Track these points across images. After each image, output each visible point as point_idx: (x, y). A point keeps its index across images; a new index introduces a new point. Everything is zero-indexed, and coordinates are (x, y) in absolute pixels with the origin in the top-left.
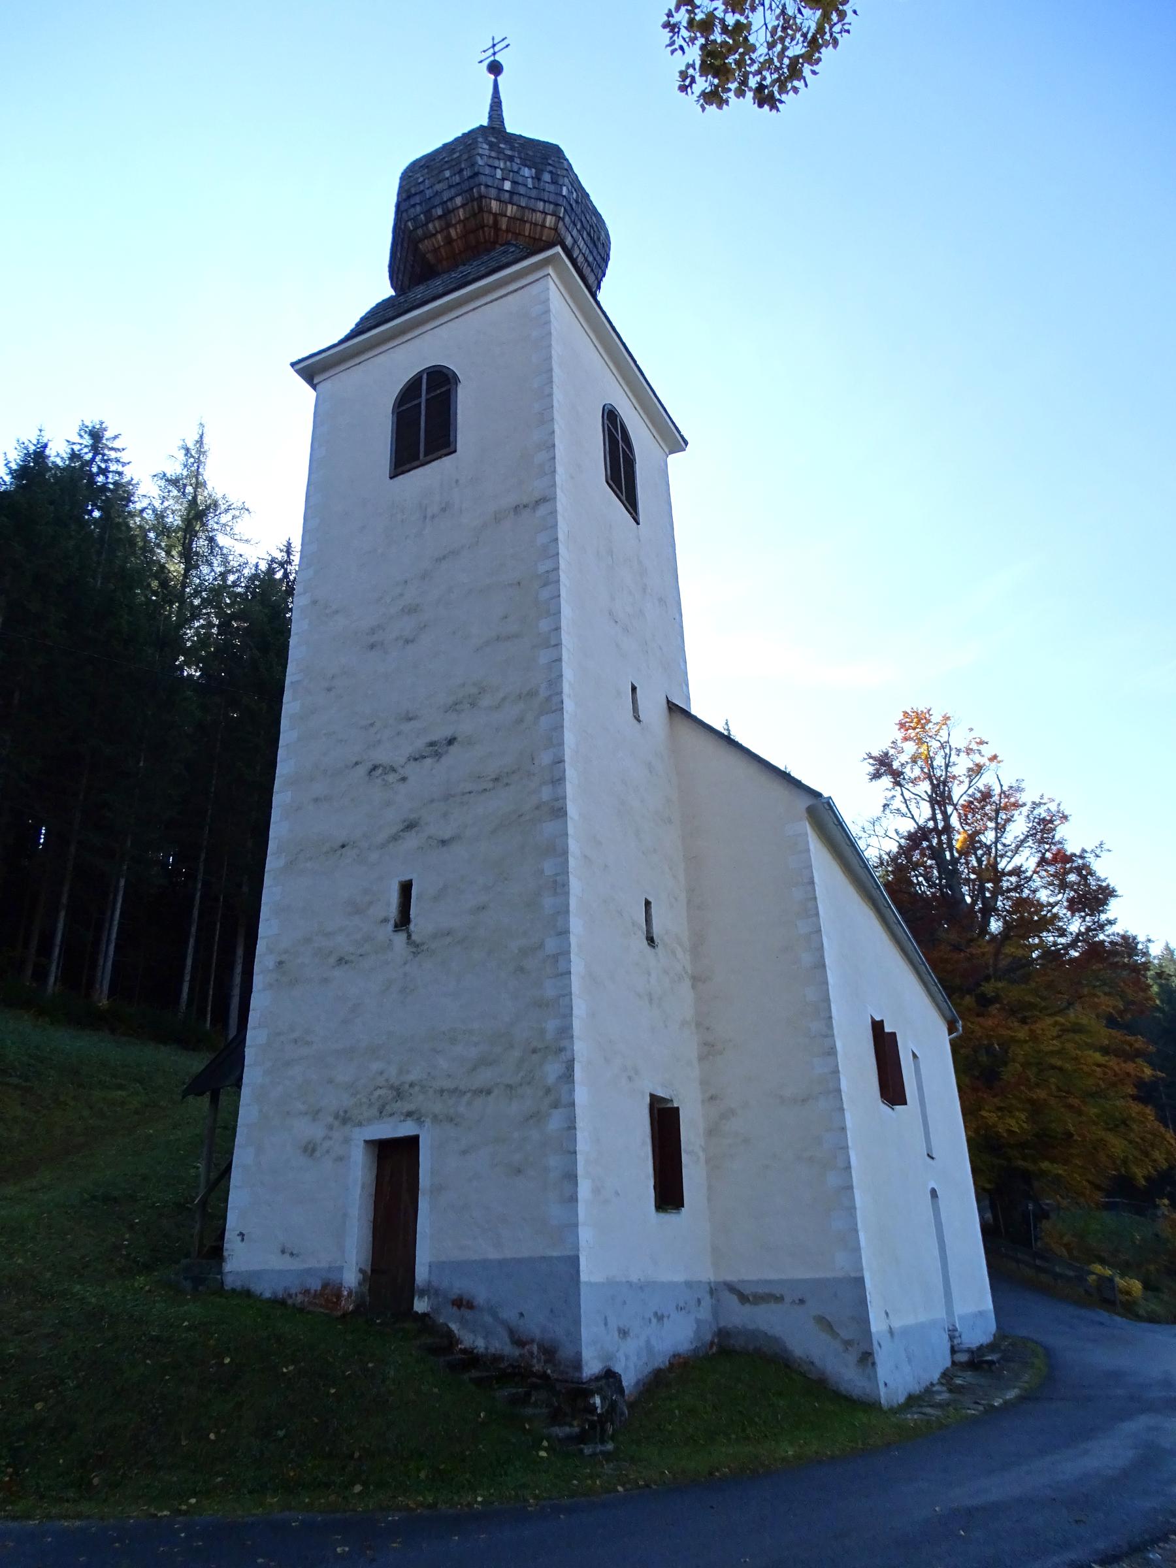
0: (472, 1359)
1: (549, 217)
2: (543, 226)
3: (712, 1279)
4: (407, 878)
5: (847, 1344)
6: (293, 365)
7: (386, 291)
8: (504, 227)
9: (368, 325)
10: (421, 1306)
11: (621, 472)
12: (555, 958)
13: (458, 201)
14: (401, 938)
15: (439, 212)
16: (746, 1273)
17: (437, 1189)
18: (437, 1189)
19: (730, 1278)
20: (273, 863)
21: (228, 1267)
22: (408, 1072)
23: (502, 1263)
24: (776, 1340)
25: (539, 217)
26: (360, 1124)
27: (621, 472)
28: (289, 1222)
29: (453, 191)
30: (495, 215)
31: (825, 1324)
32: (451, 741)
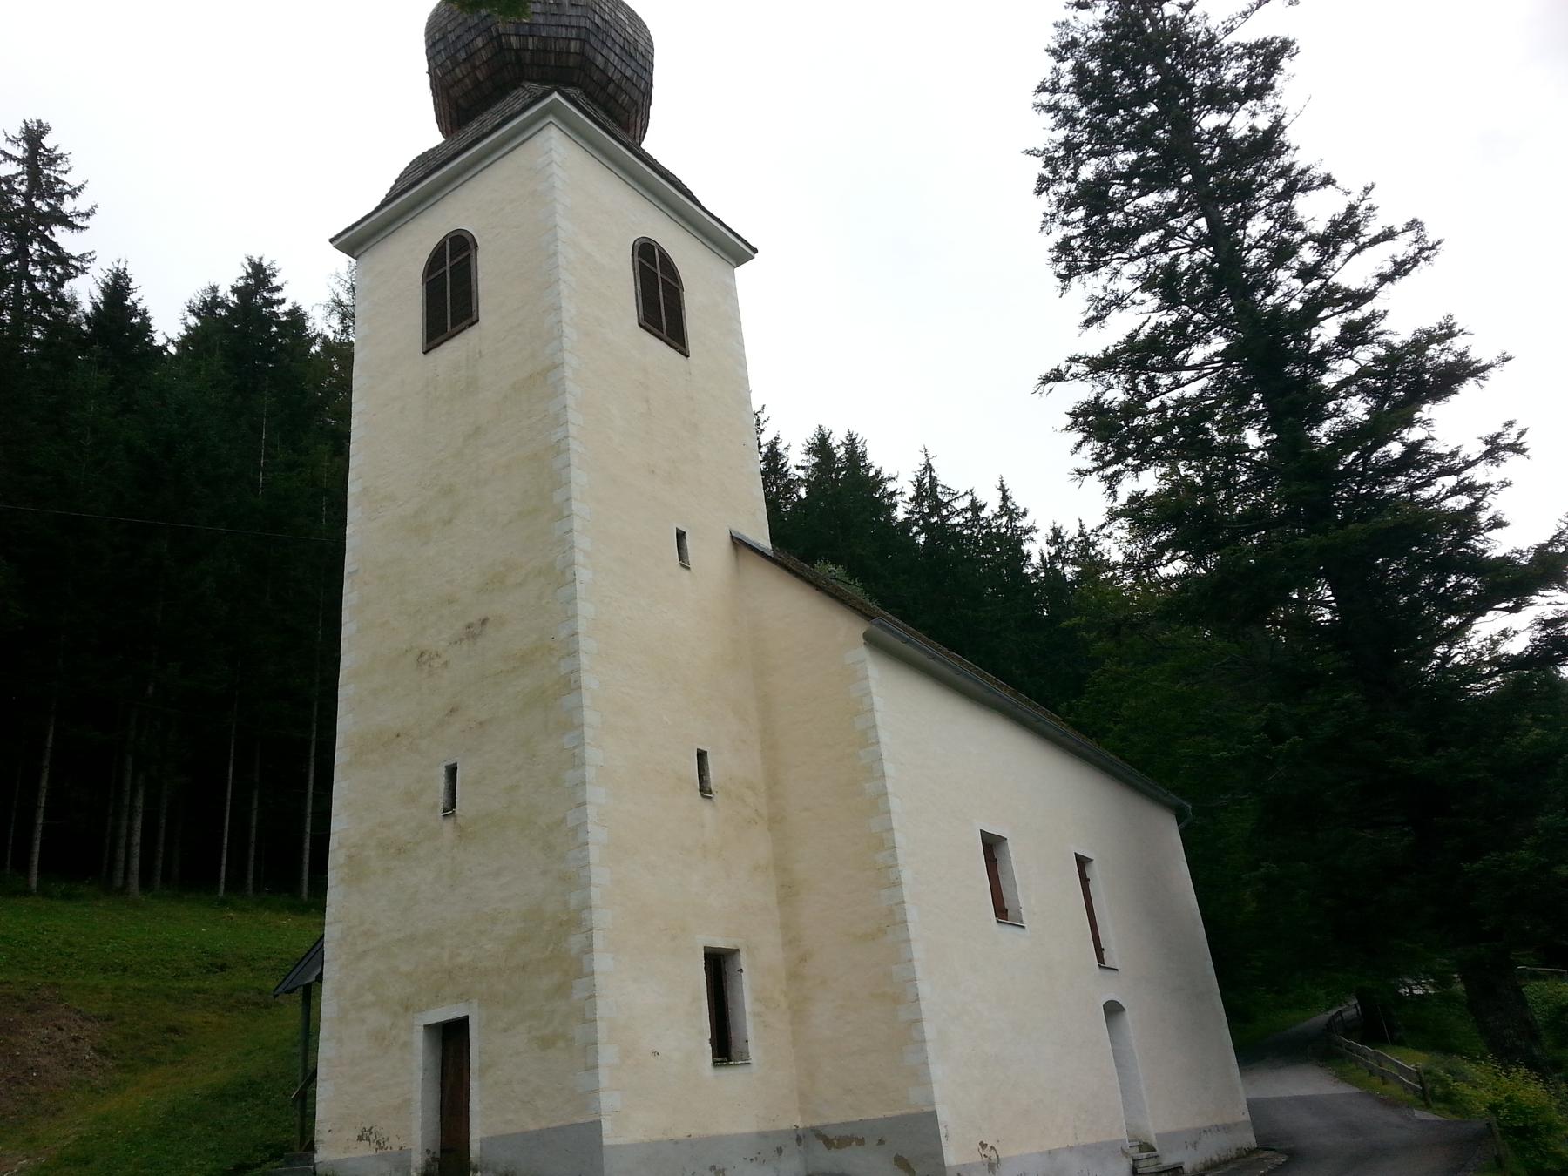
1: (573, 43)
2: (569, 53)
3: (801, 1126)
4: (451, 762)
6: (332, 241)
7: (432, 137)
8: (528, 60)
9: (410, 180)
11: (661, 304)
13: (479, 42)
14: (448, 825)
16: (834, 1115)
19: (816, 1123)
21: (318, 1158)
22: (459, 955)
23: (539, 1134)
25: (561, 45)
26: (420, 1011)
27: (661, 304)
30: (517, 50)
32: (484, 622)
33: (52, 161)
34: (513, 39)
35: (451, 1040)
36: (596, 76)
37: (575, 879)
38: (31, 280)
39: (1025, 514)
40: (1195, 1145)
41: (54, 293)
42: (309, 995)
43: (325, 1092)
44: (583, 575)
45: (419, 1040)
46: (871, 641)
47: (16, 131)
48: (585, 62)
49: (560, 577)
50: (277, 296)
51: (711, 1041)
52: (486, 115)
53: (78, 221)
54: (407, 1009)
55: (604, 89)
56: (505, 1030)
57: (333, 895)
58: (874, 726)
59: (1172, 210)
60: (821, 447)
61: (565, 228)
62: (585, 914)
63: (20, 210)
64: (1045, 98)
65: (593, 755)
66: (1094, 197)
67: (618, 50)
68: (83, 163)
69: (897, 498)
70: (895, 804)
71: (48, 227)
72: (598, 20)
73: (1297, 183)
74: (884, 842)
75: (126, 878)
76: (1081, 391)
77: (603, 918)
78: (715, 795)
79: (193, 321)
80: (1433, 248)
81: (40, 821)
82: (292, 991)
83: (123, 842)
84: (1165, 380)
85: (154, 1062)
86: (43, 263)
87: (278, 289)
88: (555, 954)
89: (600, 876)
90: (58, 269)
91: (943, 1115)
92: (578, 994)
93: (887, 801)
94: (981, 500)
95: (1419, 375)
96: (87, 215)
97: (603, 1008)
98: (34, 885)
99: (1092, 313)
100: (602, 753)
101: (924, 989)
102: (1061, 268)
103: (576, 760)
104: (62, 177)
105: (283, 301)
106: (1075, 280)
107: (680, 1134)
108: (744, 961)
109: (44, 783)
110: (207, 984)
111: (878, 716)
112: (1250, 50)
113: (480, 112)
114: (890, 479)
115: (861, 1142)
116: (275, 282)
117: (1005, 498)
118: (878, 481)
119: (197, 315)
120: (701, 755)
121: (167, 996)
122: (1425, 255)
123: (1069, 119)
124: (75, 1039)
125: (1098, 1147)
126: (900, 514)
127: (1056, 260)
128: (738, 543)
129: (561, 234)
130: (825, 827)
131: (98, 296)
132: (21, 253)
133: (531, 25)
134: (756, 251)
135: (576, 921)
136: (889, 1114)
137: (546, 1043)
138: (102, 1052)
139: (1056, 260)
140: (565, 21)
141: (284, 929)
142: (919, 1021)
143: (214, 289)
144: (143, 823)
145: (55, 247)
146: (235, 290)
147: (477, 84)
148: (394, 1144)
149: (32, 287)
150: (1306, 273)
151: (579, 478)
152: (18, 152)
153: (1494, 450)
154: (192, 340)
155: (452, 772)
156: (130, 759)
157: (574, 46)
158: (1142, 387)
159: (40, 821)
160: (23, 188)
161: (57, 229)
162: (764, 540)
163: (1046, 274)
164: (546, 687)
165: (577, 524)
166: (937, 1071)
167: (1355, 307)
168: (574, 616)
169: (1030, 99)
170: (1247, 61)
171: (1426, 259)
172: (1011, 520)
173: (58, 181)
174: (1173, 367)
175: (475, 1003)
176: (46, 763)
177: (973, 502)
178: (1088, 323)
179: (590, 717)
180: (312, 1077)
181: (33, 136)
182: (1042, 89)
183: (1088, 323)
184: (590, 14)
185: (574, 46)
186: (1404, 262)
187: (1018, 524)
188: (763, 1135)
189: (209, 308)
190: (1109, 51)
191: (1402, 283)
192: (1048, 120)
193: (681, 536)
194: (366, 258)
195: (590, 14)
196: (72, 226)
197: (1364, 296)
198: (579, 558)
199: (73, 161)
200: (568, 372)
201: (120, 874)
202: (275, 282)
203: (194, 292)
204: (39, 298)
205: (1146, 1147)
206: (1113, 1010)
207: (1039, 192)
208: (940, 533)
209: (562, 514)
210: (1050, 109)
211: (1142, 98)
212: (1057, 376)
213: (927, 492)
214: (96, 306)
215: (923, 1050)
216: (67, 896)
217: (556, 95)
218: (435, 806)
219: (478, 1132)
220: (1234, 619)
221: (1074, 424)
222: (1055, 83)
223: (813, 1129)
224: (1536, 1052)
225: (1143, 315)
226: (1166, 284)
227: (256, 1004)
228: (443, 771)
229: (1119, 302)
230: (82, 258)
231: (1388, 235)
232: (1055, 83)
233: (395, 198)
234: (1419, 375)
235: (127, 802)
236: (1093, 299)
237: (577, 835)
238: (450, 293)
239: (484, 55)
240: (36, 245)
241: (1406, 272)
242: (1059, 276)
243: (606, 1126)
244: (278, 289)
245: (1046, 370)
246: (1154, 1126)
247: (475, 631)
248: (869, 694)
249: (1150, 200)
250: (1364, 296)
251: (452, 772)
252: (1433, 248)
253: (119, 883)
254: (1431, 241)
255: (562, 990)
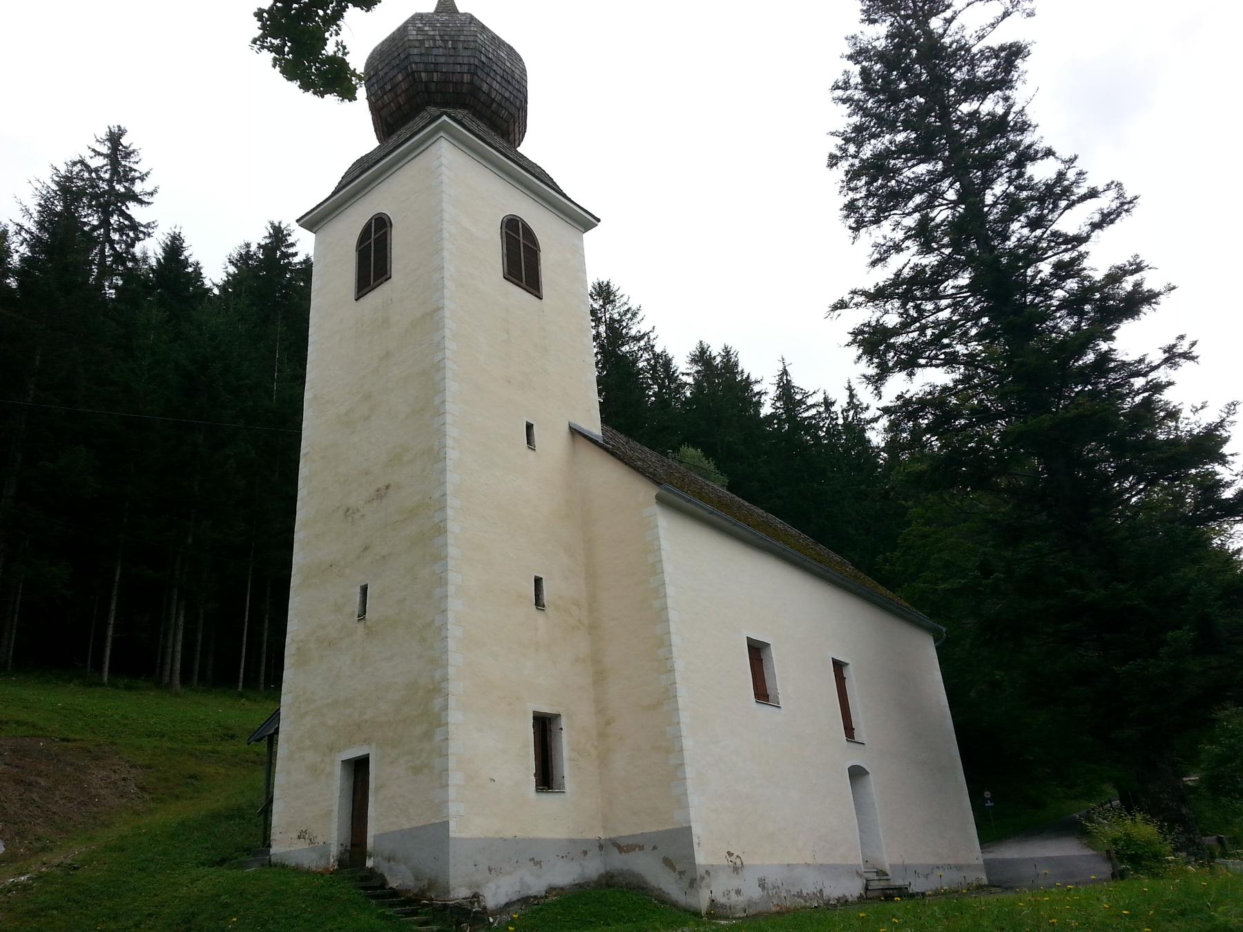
0: (394, 893)
2: (462, 82)
5: (681, 873)
9: (352, 177)
10: (370, 863)
12: (440, 629)
13: (400, 77)
14: (361, 626)
15: (388, 87)
16: (625, 830)
17: (377, 789)
18: (377, 789)
19: (613, 836)
20: (295, 581)
21: (272, 851)
24: (634, 874)
25: (456, 78)
28: (304, 819)
29: (396, 71)
31: (668, 862)
32: (387, 487)
33: (128, 155)
34: (423, 75)
35: (359, 768)
36: (483, 98)
37: (438, 661)
38: (112, 242)
39: (867, 408)
40: (927, 876)
41: (127, 252)
42: (272, 740)
43: (277, 807)
44: (452, 454)
45: (338, 770)
46: (660, 500)
47: (103, 134)
48: (475, 89)
49: (436, 456)
50: (291, 250)
51: (535, 775)
52: (403, 130)
53: (146, 199)
54: (331, 750)
55: (489, 107)
56: (392, 763)
57: (287, 675)
58: (661, 561)
59: (939, 177)
60: (702, 357)
61: (449, 210)
62: (444, 684)
63: (105, 192)
64: (839, 93)
65: (454, 577)
66: (877, 168)
67: (499, 79)
68: (151, 158)
69: (763, 398)
70: (673, 615)
71: (124, 204)
72: (483, 59)
73: (1027, 156)
74: (663, 642)
75: (171, 677)
76: (865, 315)
77: (457, 687)
78: (548, 609)
79: (232, 269)
80: (1131, 202)
81: (110, 633)
82: (259, 740)
83: (170, 650)
84: (929, 306)
85: (177, 797)
86: (121, 229)
87: (292, 245)
88: (424, 712)
89: (456, 659)
90: (131, 234)
91: (697, 830)
92: (438, 738)
93: (667, 614)
94: (832, 397)
95: (1120, 301)
96: (152, 194)
97: (454, 747)
98: (106, 679)
99: (876, 256)
100: (461, 575)
101: (687, 743)
102: (851, 222)
103: (442, 581)
104: (135, 166)
105: (295, 254)
106: (863, 231)
107: (508, 834)
108: (564, 722)
109: (113, 607)
110: (220, 748)
111: (664, 555)
112: (995, 53)
113: (398, 129)
114: (757, 382)
115: (641, 848)
116: (290, 240)
117: (852, 396)
118: (747, 383)
119: (235, 265)
120: (538, 581)
121: (191, 754)
122: (1126, 207)
123: (858, 107)
124: (124, 779)
125: (835, 867)
126: (766, 410)
127: (847, 217)
128: (575, 432)
129: (446, 216)
130: (621, 628)
131: (160, 254)
132: (105, 223)
133: (436, 64)
134: (599, 220)
135: (438, 689)
136: (661, 829)
137: (417, 770)
138: (143, 789)
139: (847, 217)
140: (460, 60)
141: (271, 706)
142: (682, 764)
143: (248, 245)
144: (184, 633)
145: (129, 218)
146: (260, 246)
147: (399, 107)
148: (320, 840)
149: (113, 248)
150: (1034, 224)
151: (452, 387)
152: (105, 149)
153: (1172, 356)
154: (233, 283)
155: (364, 589)
156: (176, 591)
157: (466, 78)
158: (913, 313)
159: (110, 633)
160: (107, 176)
161: (131, 204)
162: (594, 426)
163: (840, 227)
164: (426, 532)
165: (449, 419)
166: (694, 800)
167: (1073, 248)
168: (444, 483)
169: (829, 95)
170: (994, 61)
171: (1127, 211)
172: (856, 413)
173: (131, 170)
174: (936, 296)
175: (374, 745)
176: (115, 592)
177: (826, 399)
178: (874, 263)
179: (452, 551)
180: (270, 801)
181: (115, 138)
182: (836, 87)
183: (874, 263)
184: (478, 54)
185: (466, 78)
186: (1110, 214)
187: (862, 416)
188: (572, 841)
189: (244, 260)
190: (890, 59)
191: (1109, 230)
192: (845, 109)
193: (529, 427)
194: (321, 233)
195: (478, 54)
196: (141, 202)
197: (1079, 240)
198: (449, 442)
199: (143, 154)
200: (447, 313)
201: (167, 673)
202: (290, 240)
203: (233, 248)
204: (119, 258)
205: (881, 873)
206: (857, 774)
207: (831, 166)
208: (800, 426)
209: (440, 412)
210: (844, 101)
211: (911, 92)
212: (842, 305)
213: (786, 390)
214: (158, 260)
215: (684, 784)
216: (128, 688)
217: (445, 118)
218: (354, 612)
219: (373, 830)
220: (983, 490)
221: (854, 341)
222: (846, 83)
223: (610, 840)
224: (1184, 811)
225: (909, 259)
226: (924, 234)
227: (255, 762)
228: (358, 590)
229: (898, 248)
230: (148, 226)
231: (1093, 194)
232: (846, 83)
233: (344, 187)
234: (1120, 301)
235: (173, 621)
236: (876, 245)
237: (441, 632)
238: (373, 260)
239: (403, 86)
240: (115, 217)
241: (1112, 222)
242: (851, 228)
243: (452, 824)
244: (292, 245)
245: (835, 300)
246: (891, 855)
247: (381, 494)
248: (658, 538)
249: (922, 169)
250: (1079, 240)
251: (364, 589)
252: (1131, 202)
253: (166, 679)
254: (1129, 196)
255: (428, 735)
